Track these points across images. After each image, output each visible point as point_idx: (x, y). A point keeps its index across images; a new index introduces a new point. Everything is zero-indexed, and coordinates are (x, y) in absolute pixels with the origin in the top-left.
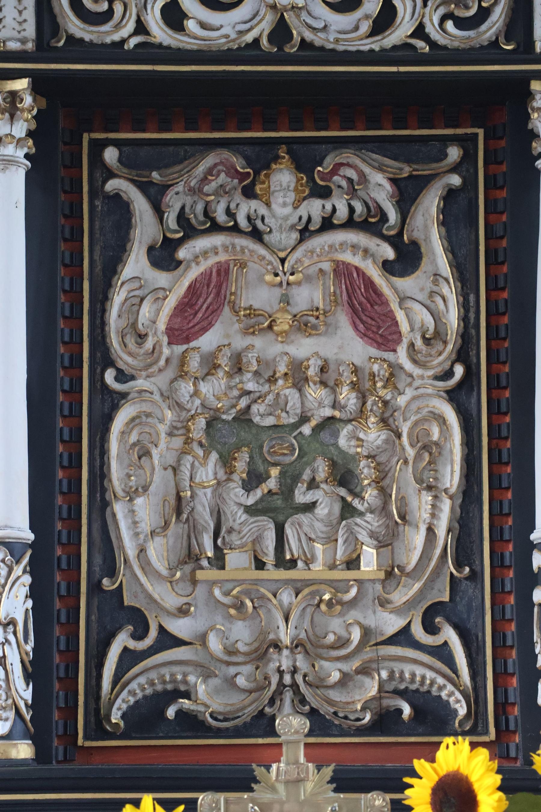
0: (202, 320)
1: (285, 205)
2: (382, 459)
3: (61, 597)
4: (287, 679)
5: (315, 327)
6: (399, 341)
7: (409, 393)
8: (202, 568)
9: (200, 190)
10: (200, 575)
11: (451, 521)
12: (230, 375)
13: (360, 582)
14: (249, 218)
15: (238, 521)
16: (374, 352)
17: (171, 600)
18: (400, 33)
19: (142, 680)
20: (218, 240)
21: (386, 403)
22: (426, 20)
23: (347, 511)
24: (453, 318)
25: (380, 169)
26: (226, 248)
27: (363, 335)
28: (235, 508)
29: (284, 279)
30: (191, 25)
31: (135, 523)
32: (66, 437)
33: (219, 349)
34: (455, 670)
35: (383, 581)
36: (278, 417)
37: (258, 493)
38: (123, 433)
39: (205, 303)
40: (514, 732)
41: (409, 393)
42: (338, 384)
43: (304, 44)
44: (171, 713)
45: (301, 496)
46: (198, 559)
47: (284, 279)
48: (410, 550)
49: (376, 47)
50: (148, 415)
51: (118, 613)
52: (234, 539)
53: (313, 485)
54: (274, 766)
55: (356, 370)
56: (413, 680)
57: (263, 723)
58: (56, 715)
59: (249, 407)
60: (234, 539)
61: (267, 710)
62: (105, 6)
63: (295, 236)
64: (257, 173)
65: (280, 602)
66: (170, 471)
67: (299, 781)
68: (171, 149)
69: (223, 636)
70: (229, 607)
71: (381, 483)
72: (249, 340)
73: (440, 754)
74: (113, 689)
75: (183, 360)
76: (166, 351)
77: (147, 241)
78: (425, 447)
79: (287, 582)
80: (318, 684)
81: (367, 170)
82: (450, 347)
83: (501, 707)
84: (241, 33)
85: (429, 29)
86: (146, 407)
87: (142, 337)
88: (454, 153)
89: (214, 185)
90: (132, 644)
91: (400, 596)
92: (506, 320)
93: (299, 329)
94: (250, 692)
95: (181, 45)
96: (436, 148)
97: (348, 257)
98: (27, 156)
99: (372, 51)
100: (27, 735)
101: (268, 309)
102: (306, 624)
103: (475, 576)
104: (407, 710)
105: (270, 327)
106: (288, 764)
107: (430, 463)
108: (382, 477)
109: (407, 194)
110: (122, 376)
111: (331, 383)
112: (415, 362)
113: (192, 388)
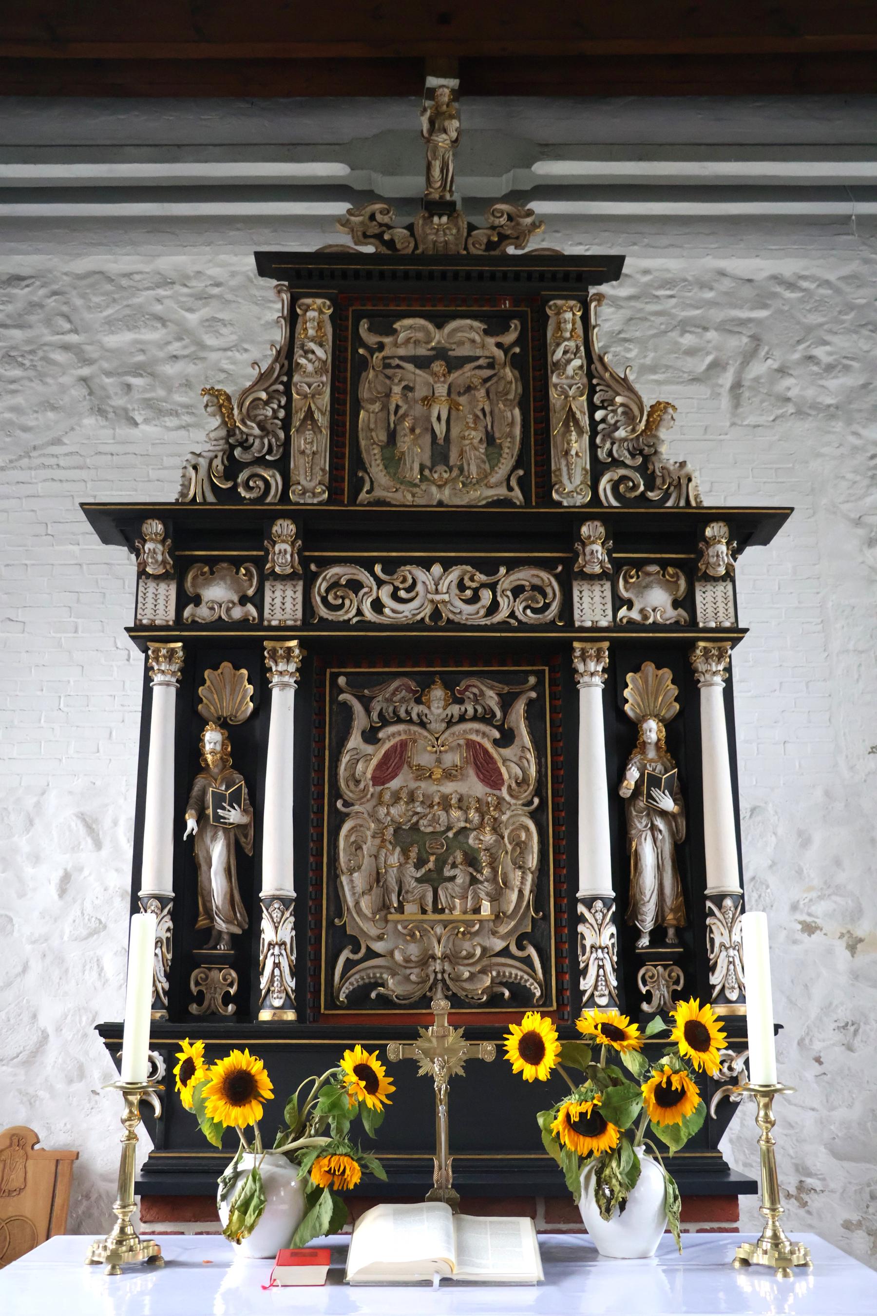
0: (392, 772)
1: (438, 708)
2: (493, 851)
3: (311, 929)
4: (439, 976)
5: (455, 776)
6: (503, 783)
7: (509, 813)
8: (391, 913)
9: (391, 700)
10: (390, 917)
11: (532, 886)
12: (407, 803)
13: (481, 921)
14: (418, 715)
15: (412, 887)
16: (488, 790)
17: (372, 930)
18: (502, 614)
19: (357, 976)
20: (401, 727)
21: (495, 819)
22: (516, 609)
23: (474, 881)
24: (533, 771)
25: (492, 688)
26: (405, 732)
27: (482, 781)
28: (410, 879)
29: (438, 749)
30: (387, 611)
31: (353, 887)
32: (315, 839)
33: (401, 788)
34: (534, 970)
35: (494, 921)
36: (435, 827)
37: (423, 870)
38: (346, 836)
39: (393, 763)
40: (567, 1005)
41: (509, 813)
42: (468, 808)
44: (373, 995)
45: (448, 872)
46: (389, 908)
47: (438, 749)
48: (509, 903)
49: (488, 623)
50: (361, 826)
51: (345, 938)
52: (410, 897)
53: (454, 866)
54: (430, 1028)
55: (478, 800)
56: (510, 976)
57: (425, 1001)
58: (309, 996)
59: (418, 821)
60: (410, 897)
61: (428, 994)
62: (340, 601)
63: (444, 725)
64: (423, 690)
65: (436, 933)
66: (373, 858)
67: (444, 1036)
68: (375, 677)
69: (403, 952)
70: (406, 935)
71: (493, 865)
72: (418, 784)
73: (525, 1021)
74: (341, 981)
75: (381, 795)
76: (371, 790)
77: (362, 728)
78: (518, 844)
80: (457, 979)
81: (484, 689)
82: (531, 787)
83: (560, 991)
84: (414, 615)
85: (517, 613)
86: (359, 821)
87: (358, 782)
88: (532, 680)
91: (504, 929)
92: (562, 772)
93: (446, 777)
94: (418, 983)
95: (381, 622)
97: (474, 737)
98: (295, 682)
99: (486, 625)
100: (292, 1007)
101: (429, 766)
102: (450, 945)
103: (546, 917)
104: (507, 993)
105: (430, 776)
106: (438, 1027)
107: (520, 853)
108: (79, 913)
110: (346, 804)
111: (465, 808)
112: (511, 796)
113: (386, 811)
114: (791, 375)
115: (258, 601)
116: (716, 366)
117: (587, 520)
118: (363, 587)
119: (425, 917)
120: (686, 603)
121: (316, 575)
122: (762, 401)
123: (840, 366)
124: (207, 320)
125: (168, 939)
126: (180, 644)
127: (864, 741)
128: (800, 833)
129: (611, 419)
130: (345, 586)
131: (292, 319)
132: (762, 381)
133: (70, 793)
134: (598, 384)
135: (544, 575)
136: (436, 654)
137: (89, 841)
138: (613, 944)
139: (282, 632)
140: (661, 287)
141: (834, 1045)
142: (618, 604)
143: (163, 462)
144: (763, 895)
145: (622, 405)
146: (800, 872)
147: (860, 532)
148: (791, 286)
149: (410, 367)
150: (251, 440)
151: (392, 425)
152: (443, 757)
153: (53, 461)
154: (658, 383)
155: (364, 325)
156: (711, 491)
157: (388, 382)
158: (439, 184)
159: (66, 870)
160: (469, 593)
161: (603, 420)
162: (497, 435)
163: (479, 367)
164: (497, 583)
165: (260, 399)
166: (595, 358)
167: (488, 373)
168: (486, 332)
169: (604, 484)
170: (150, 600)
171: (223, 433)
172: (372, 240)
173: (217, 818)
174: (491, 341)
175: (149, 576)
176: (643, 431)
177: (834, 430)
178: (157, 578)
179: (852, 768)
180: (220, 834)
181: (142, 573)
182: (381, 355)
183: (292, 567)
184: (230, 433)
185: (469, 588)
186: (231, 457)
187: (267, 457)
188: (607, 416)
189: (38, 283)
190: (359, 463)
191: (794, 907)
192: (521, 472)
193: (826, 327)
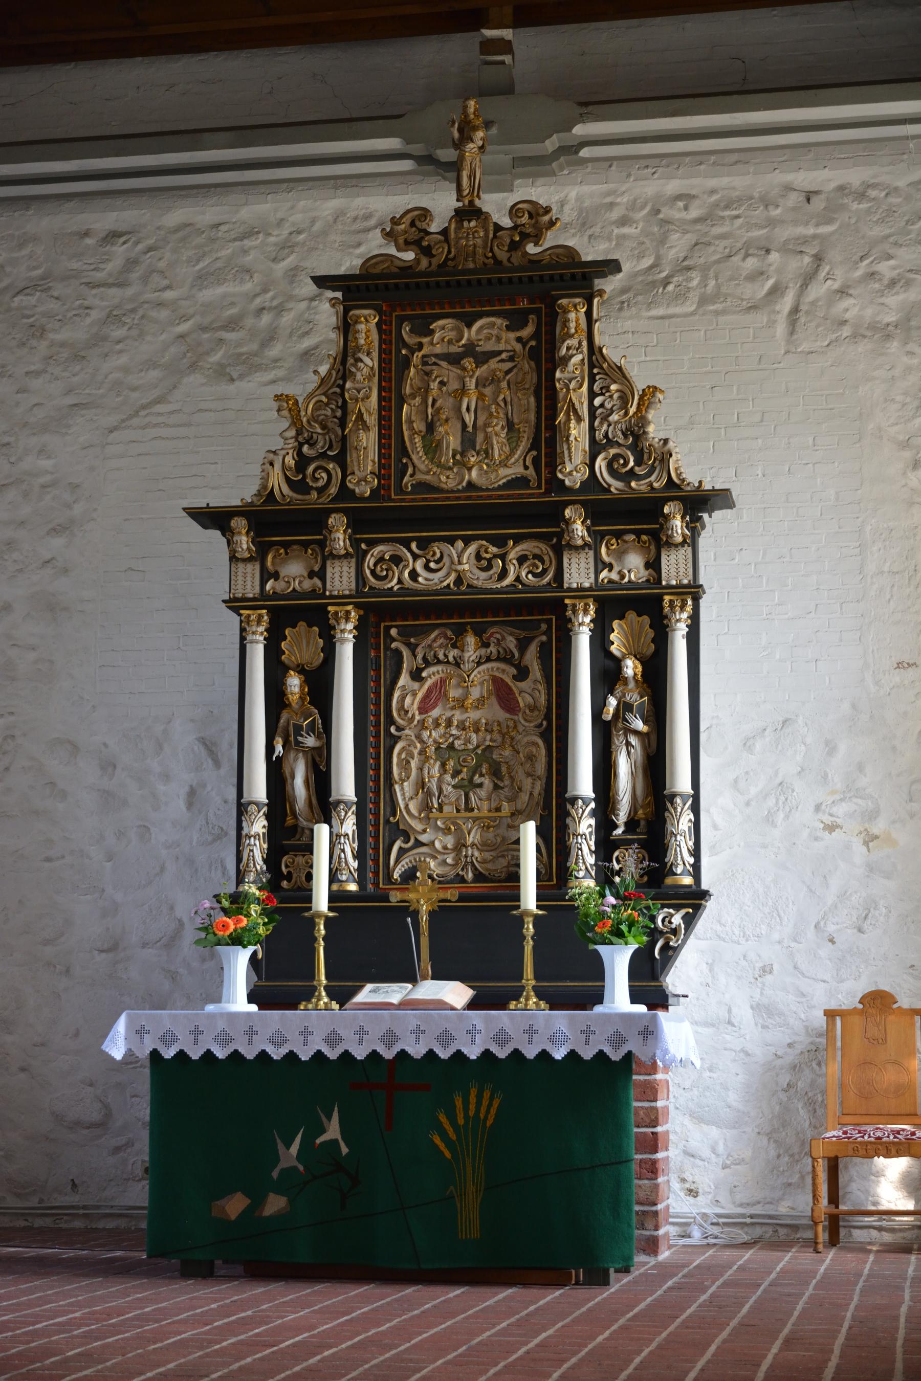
10: (431, 815)
14: (454, 657)
16: (508, 716)
17: (418, 827)
20: (440, 668)
23: (496, 787)
24: (543, 700)
25: (511, 634)
37: (457, 780)
39: (434, 695)
43: (469, 586)
45: (477, 779)
49: (499, 586)
53: (481, 775)
62: (385, 573)
79: (469, 818)
81: (505, 635)
88: (544, 627)
89: (439, 643)
90: (404, 846)
94: (453, 865)
96: (536, 625)
108: (204, 822)
109: (523, 645)
110: (399, 729)
114: (851, 295)
115: (321, 575)
116: (776, 291)
117: (571, 504)
118: (402, 561)
119: (459, 815)
120: (654, 565)
121: (365, 553)
122: (817, 327)
123: (903, 281)
124: (291, 270)
125: (264, 834)
126: (265, 611)
127: (891, 657)
128: (827, 743)
129: (608, 405)
130: (389, 560)
131: (346, 327)
132: (820, 303)
133: (192, 721)
134: (599, 373)
135: (543, 546)
136: (460, 612)
137: (210, 761)
138: (591, 833)
139: (341, 599)
140: (727, 207)
141: (846, 927)
142: (600, 566)
143: (245, 461)
144: (790, 797)
145: (617, 391)
146: (825, 777)
147: (908, 454)
148: (861, 196)
149: (444, 364)
150: (315, 436)
151: (430, 417)
152: (449, 698)
153: (161, 419)
154: (717, 313)
155: (406, 328)
156: (762, 421)
157: (426, 378)
158: (467, 191)
159: (191, 786)
160: (484, 563)
161: (602, 405)
162: (516, 420)
163: (502, 361)
164: (506, 554)
165: (321, 401)
166: (596, 350)
167: (509, 365)
168: (508, 328)
169: (600, 463)
170: (240, 578)
171: (292, 433)
172: (413, 247)
173: (298, 743)
174: (512, 335)
175: (238, 559)
176: (635, 413)
177: (889, 351)
178: (244, 560)
179: (877, 683)
180: (301, 755)
181: (233, 558)
182: (420, 354)
183: (346, 549)
184: (299, 433)
185: (485, 558)
186: (300, 453)
187: (329, 453)
188: (604, 401)
189: (134, 239)
190: (404, 451)
191: (818, 808)
192: (534, 453)
193: (891, 239)
